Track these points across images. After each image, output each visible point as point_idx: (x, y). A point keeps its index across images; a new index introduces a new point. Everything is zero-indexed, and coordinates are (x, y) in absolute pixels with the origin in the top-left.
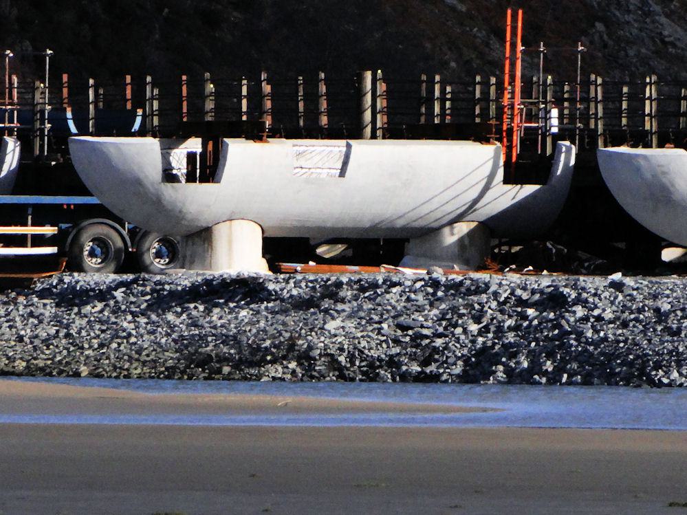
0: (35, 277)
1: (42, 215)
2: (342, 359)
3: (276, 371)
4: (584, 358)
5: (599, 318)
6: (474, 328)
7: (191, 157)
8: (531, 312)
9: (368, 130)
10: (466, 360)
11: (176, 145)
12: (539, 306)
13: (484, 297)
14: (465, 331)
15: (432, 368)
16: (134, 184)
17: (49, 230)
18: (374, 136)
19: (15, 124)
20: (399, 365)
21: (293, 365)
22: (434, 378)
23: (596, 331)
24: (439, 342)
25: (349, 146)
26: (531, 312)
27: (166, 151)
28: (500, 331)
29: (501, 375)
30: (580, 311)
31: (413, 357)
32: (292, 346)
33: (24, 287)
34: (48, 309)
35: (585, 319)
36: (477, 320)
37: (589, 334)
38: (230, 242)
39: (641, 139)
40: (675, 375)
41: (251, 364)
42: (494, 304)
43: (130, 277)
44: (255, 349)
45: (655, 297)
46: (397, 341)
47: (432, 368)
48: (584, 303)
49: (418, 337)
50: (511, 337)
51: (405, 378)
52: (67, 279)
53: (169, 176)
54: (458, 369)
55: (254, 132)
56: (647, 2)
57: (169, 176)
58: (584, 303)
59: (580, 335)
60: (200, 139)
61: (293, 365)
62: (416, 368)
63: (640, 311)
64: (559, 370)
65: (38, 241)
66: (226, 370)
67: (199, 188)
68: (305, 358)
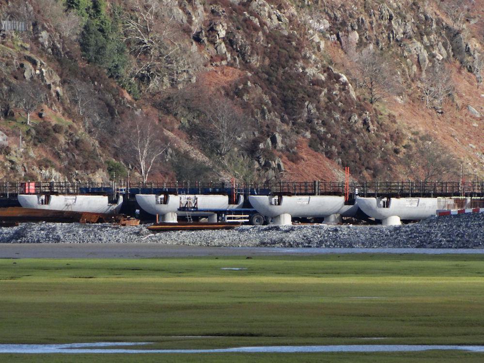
0: (235, 226)
1: (245, 213)
2: (291, 243)
3: (277, 245)
4: (341, 242)
5: (344, 234)
6: (319, 236)
7: (384, 202)
8: (331, 233)
9: (317, 194)
10: (317, 243)
11: (381, 199)
12: (333, 231)
13: (321, 230)
14: (317, 237)
15: (310, 245)
16: (263, 207)
17: (248, 216)
18: (318, 195)
19: (243, 193)
20: (303, 244)
21: (281, 244)
22: (310, 247)
23: (343, 237)
24: (312, 239)
25: (76, 197)
26: (331, 233)
27: (38, 198)
28: (324, 237)
29: (324, 246)
30: (340, 232)
31: (306, 243)
32: (282, 240)
33: (233, 228)
34: (236, 233)
35: (341, 234)
36: (320, 234)
37: (342, 237)
38: (284, 218)
39: (254, 195)
40: (357, 246)
41: (273, 244)
42: (323, 231)
43: (254, 226)
44: (275, 241)
45: (356, 229)
46: (303, 239)
47: (310, 245)
48: (341, 231)
49: (307, 239)
50: (326, 238)
51: (304, 247)
52: (241, 227)
53: (157, 203)
54: (315, 245)
55: (57, 194)
56: (1, 179)
57: (271, 204)
58: (341, 231)
59: (340, 237)
60: (283, 196)
61: (281, 244)
62: (307, 245)
63: (353, 232)
64: (335, 245)
65: (245, 218)
66: (268, 245)
67: (163, 205)
68: (284, 243)
